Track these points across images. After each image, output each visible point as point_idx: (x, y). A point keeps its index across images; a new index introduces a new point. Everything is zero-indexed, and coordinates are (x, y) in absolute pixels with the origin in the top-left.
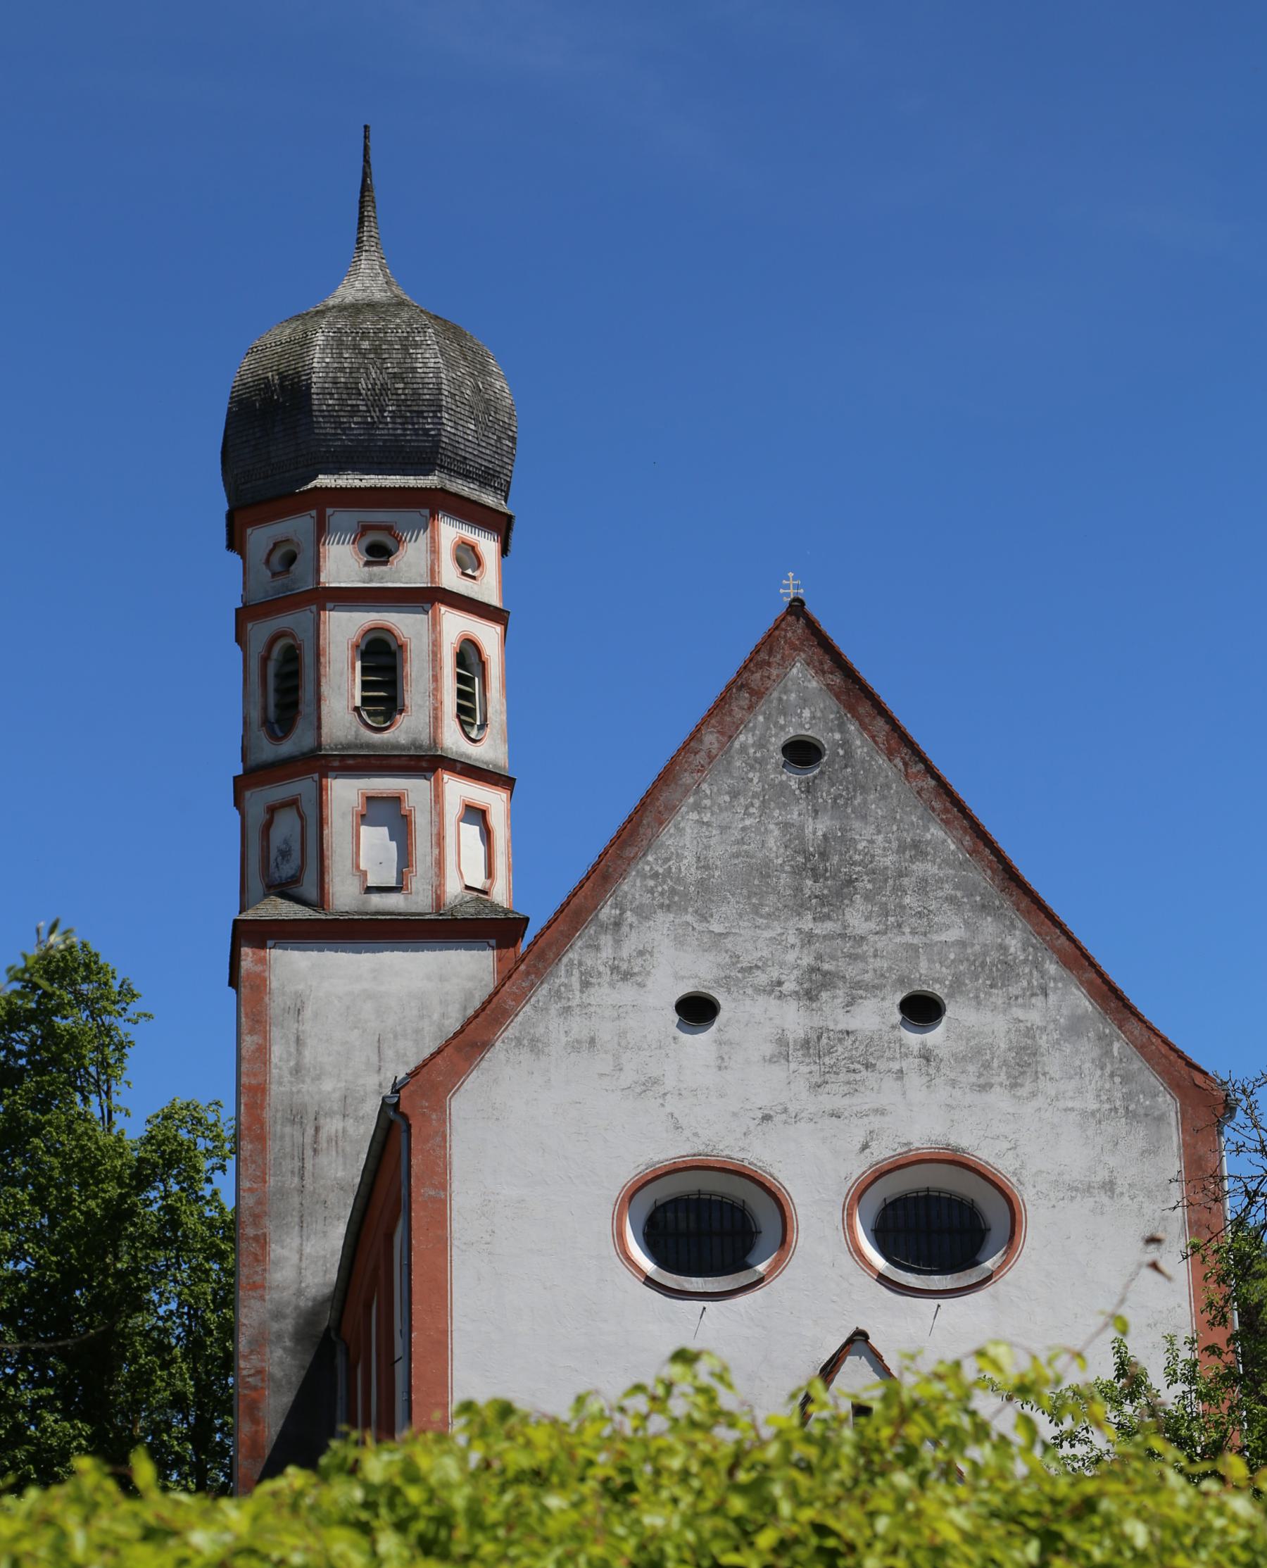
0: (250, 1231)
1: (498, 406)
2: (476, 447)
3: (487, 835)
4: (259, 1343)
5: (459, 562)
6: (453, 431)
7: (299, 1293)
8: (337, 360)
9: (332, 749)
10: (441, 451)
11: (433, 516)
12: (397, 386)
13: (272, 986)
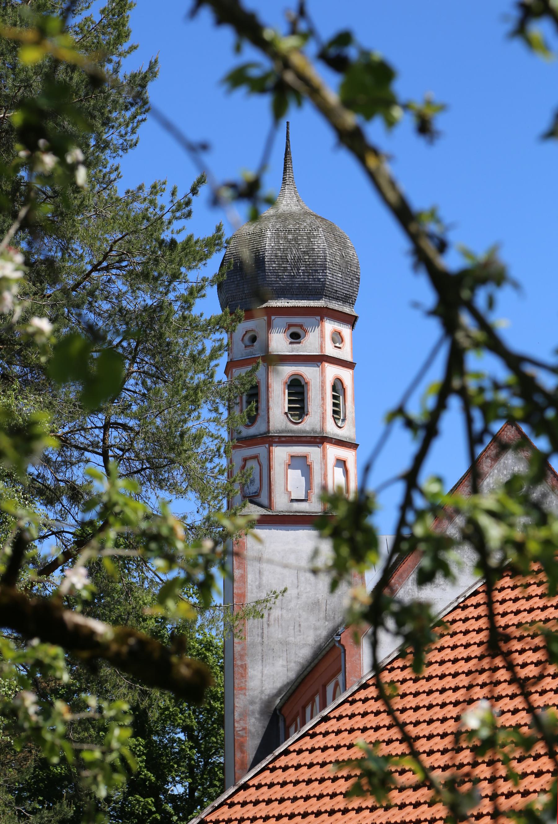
0: (239, 663)
1: (352, 264)
2: (341, 285)
3: (346, 472)
4: (244, 715)
5: (334, 341)
6: (331, 278)
7: (262, 692)
8: (277, 245)
9: (274, 433)
10: (326, 288)
11: (322, 319)
12: (305, 257)
13: (248, 546)
